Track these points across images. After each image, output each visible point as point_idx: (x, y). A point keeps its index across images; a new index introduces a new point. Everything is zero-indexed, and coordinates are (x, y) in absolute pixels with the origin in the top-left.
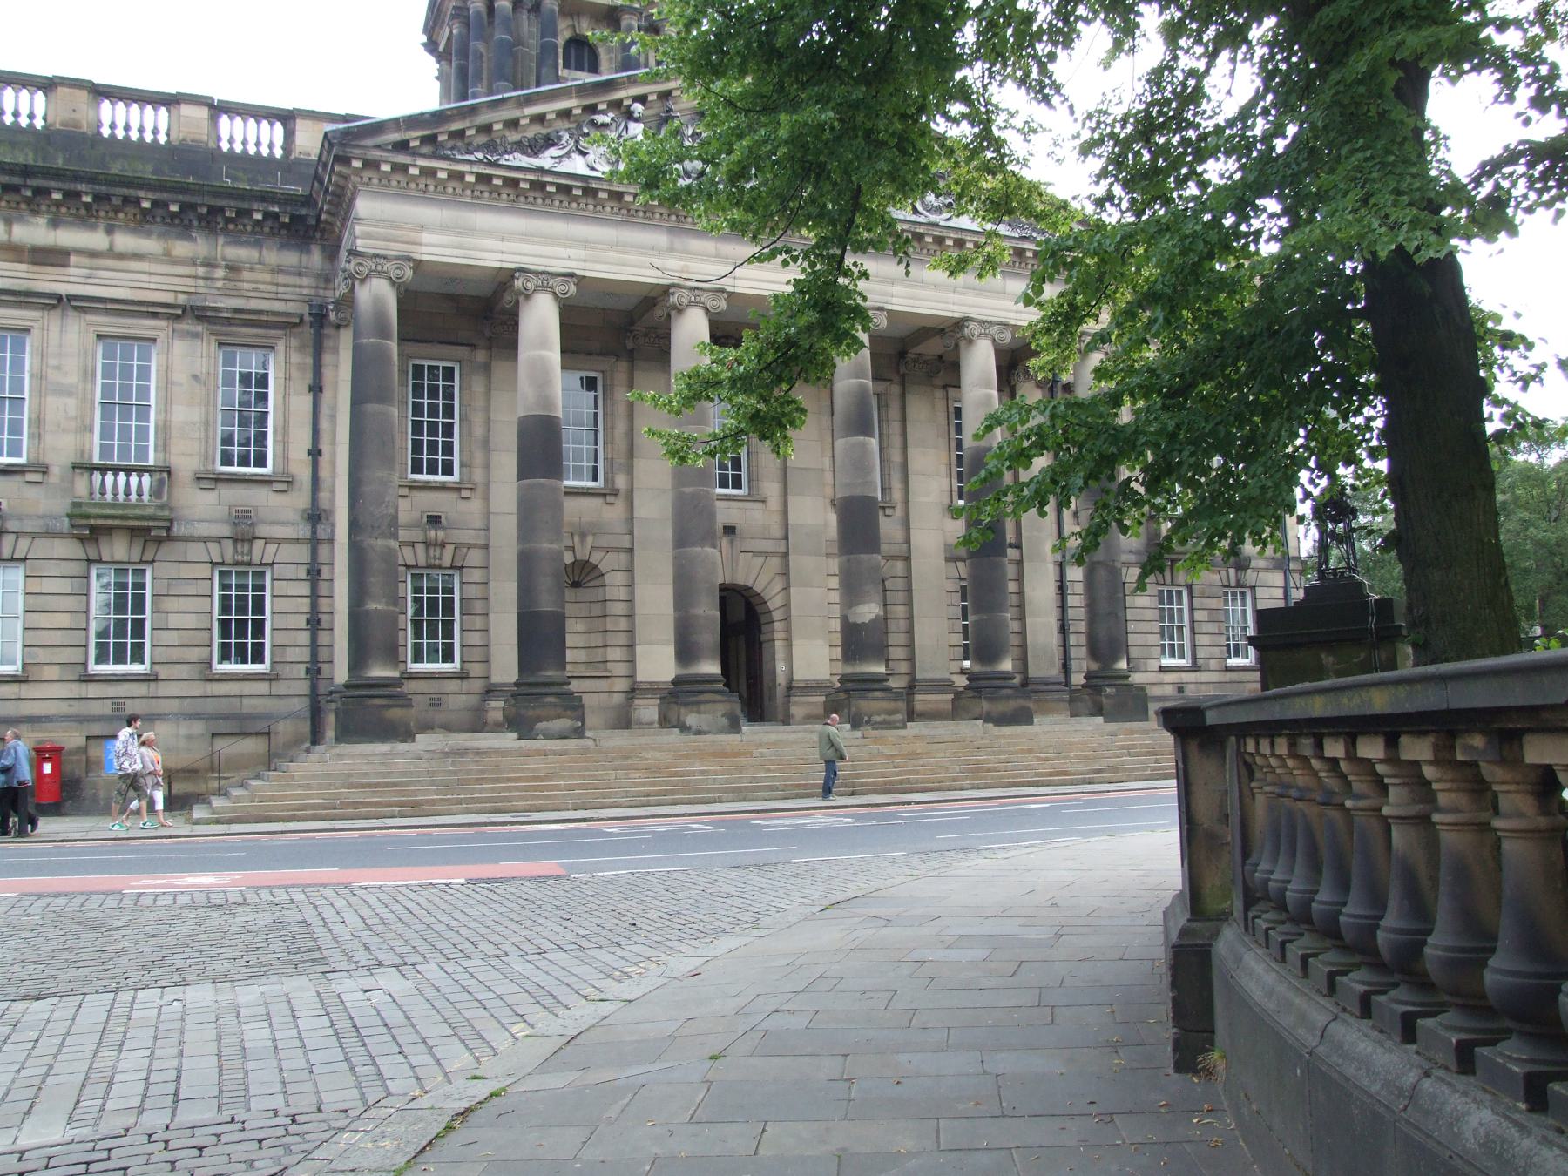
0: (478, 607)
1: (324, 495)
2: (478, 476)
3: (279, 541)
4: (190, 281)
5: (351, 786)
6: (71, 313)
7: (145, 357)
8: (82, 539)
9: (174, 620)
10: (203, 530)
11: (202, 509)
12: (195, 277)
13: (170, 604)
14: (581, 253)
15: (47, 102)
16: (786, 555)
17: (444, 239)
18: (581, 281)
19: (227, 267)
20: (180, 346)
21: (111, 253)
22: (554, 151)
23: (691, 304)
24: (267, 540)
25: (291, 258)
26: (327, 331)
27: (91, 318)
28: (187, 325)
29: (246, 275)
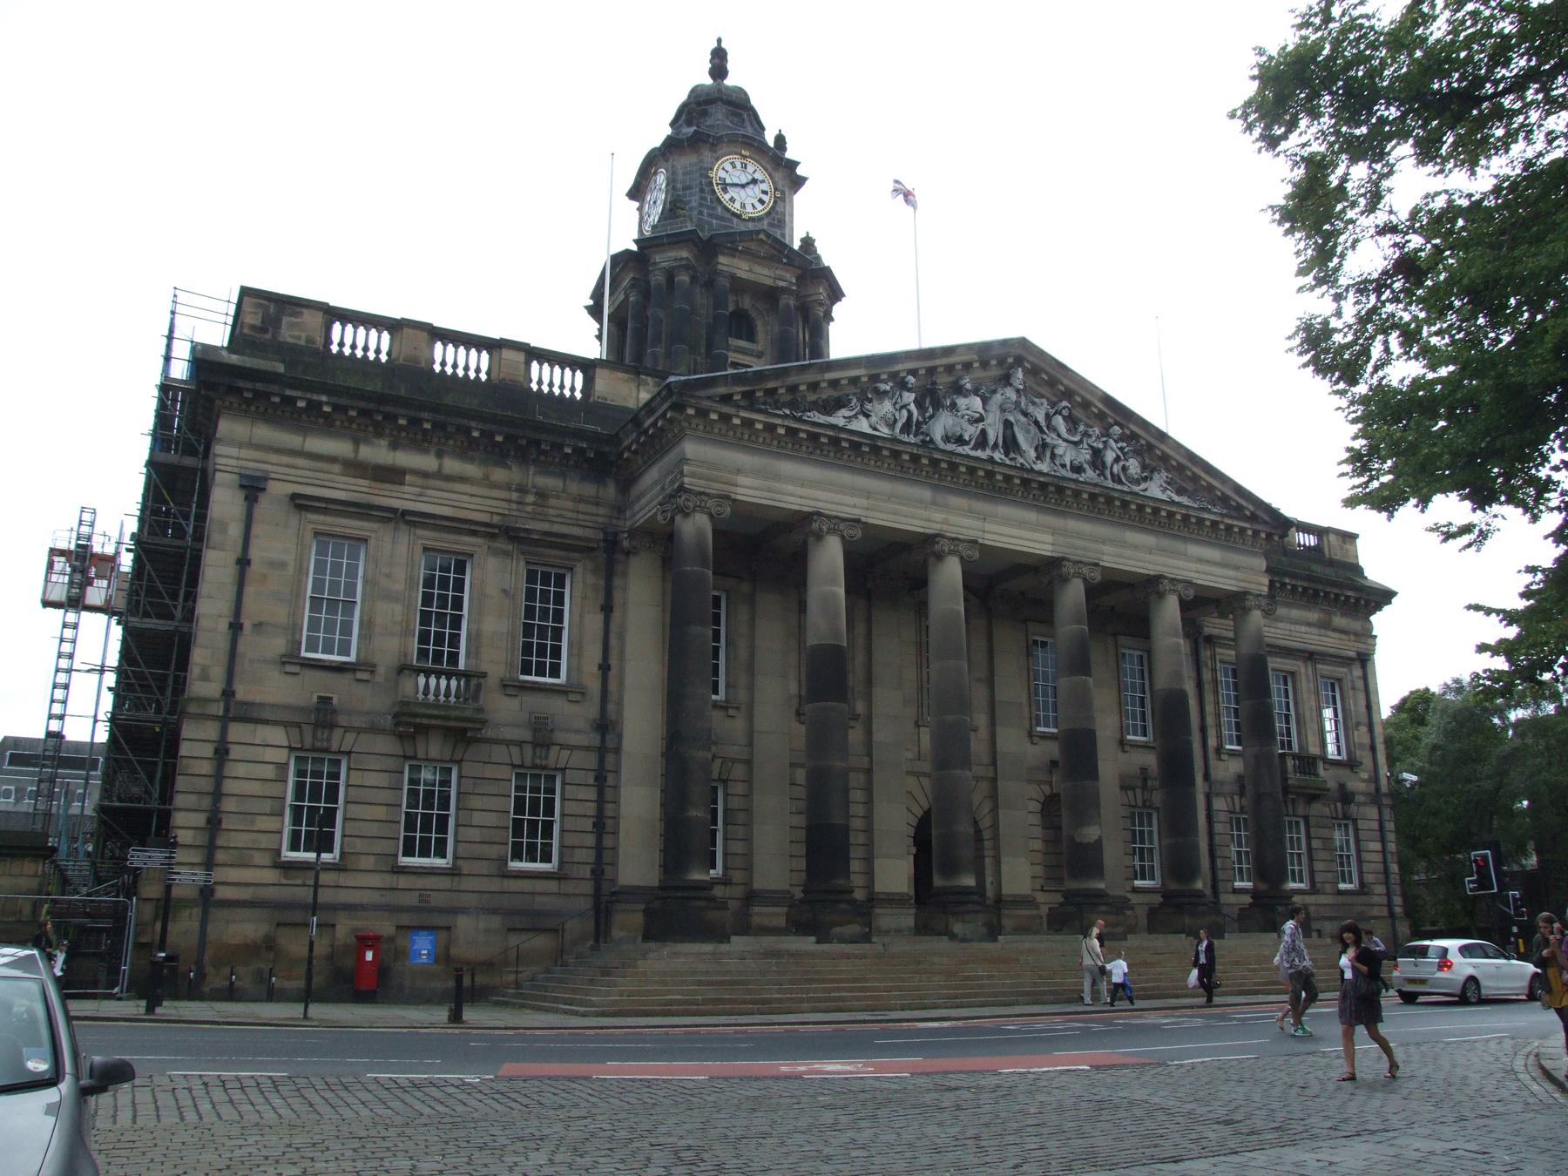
0: (741, 817)
1: (611, 707)
2: (742, 696)
3: (572, 748)
4: (504, 504)
5: (700, 983)
6: (403, 527)
7: (354, 556)
8: (401, 737)
9: (478, 818)
10: (508, 733)
11: (505, 712)
12: (509, 501)
13: (476, 802)
14: (864, 502)
15: (392, 340)
16: (994, 780)
17: (757, 482)
18: (986, 550)
19: (537, 494)
20: (492, 563)
21: (439, 475)
22: (845, 412)
23: (951, 552)
24: (563, 747)
25: (589, 489)
26: (619, 557)
27: (420, 532)
28: (501, 544)
29: (552, 502)
